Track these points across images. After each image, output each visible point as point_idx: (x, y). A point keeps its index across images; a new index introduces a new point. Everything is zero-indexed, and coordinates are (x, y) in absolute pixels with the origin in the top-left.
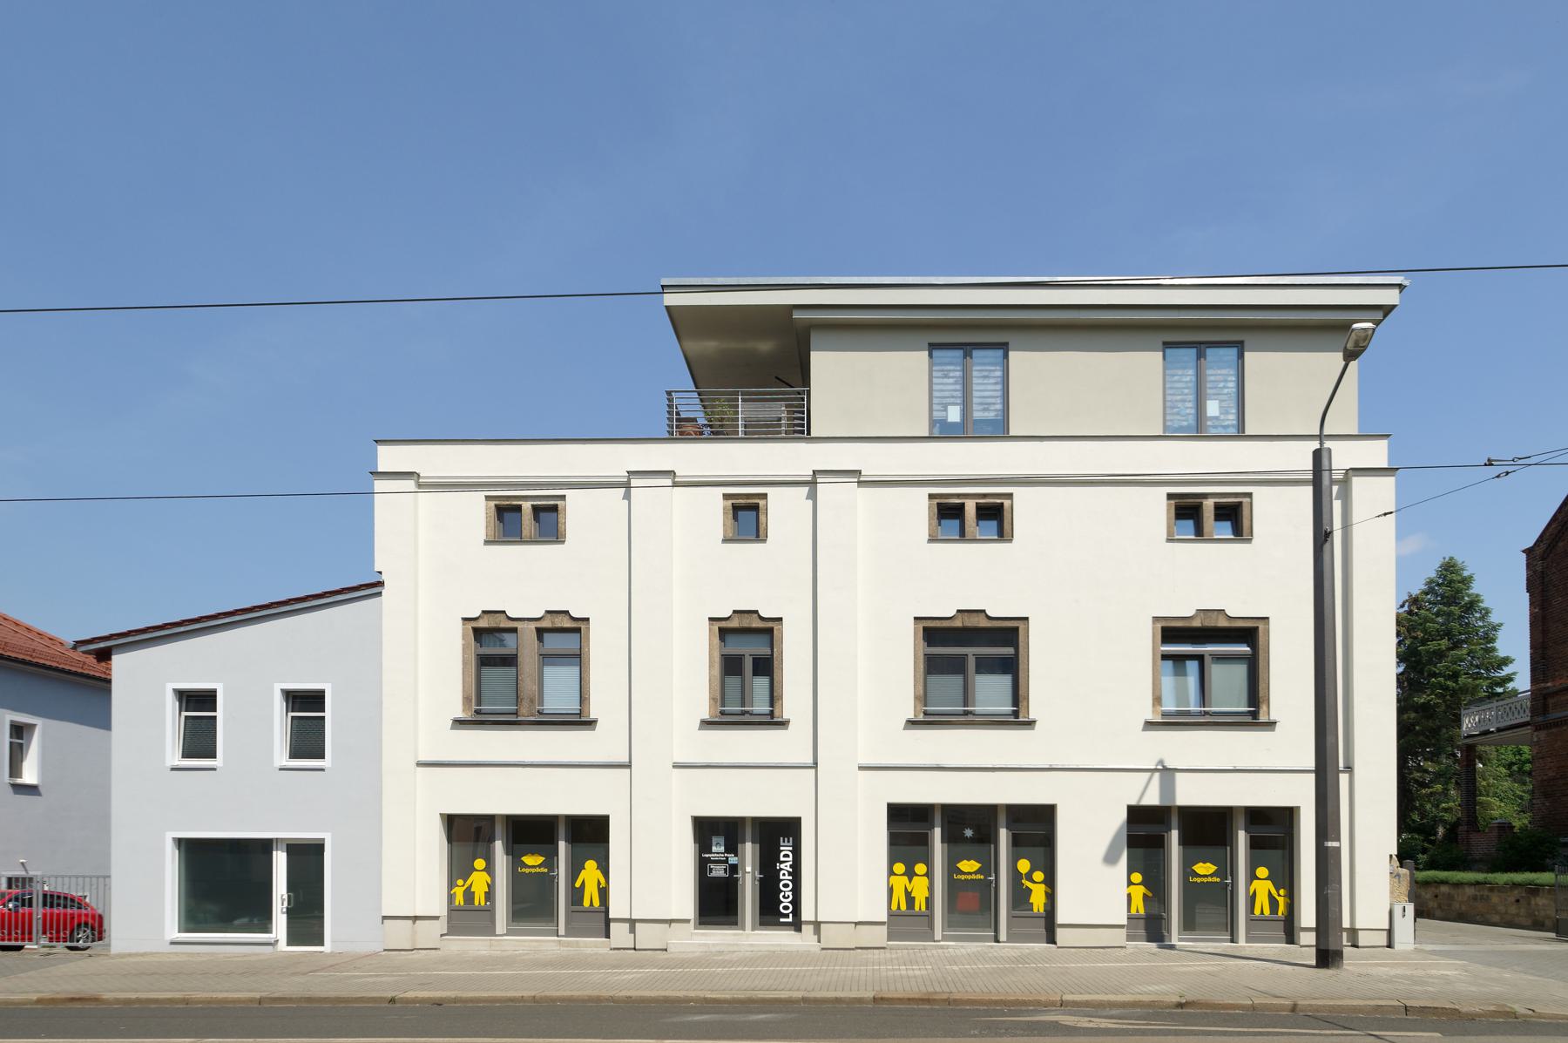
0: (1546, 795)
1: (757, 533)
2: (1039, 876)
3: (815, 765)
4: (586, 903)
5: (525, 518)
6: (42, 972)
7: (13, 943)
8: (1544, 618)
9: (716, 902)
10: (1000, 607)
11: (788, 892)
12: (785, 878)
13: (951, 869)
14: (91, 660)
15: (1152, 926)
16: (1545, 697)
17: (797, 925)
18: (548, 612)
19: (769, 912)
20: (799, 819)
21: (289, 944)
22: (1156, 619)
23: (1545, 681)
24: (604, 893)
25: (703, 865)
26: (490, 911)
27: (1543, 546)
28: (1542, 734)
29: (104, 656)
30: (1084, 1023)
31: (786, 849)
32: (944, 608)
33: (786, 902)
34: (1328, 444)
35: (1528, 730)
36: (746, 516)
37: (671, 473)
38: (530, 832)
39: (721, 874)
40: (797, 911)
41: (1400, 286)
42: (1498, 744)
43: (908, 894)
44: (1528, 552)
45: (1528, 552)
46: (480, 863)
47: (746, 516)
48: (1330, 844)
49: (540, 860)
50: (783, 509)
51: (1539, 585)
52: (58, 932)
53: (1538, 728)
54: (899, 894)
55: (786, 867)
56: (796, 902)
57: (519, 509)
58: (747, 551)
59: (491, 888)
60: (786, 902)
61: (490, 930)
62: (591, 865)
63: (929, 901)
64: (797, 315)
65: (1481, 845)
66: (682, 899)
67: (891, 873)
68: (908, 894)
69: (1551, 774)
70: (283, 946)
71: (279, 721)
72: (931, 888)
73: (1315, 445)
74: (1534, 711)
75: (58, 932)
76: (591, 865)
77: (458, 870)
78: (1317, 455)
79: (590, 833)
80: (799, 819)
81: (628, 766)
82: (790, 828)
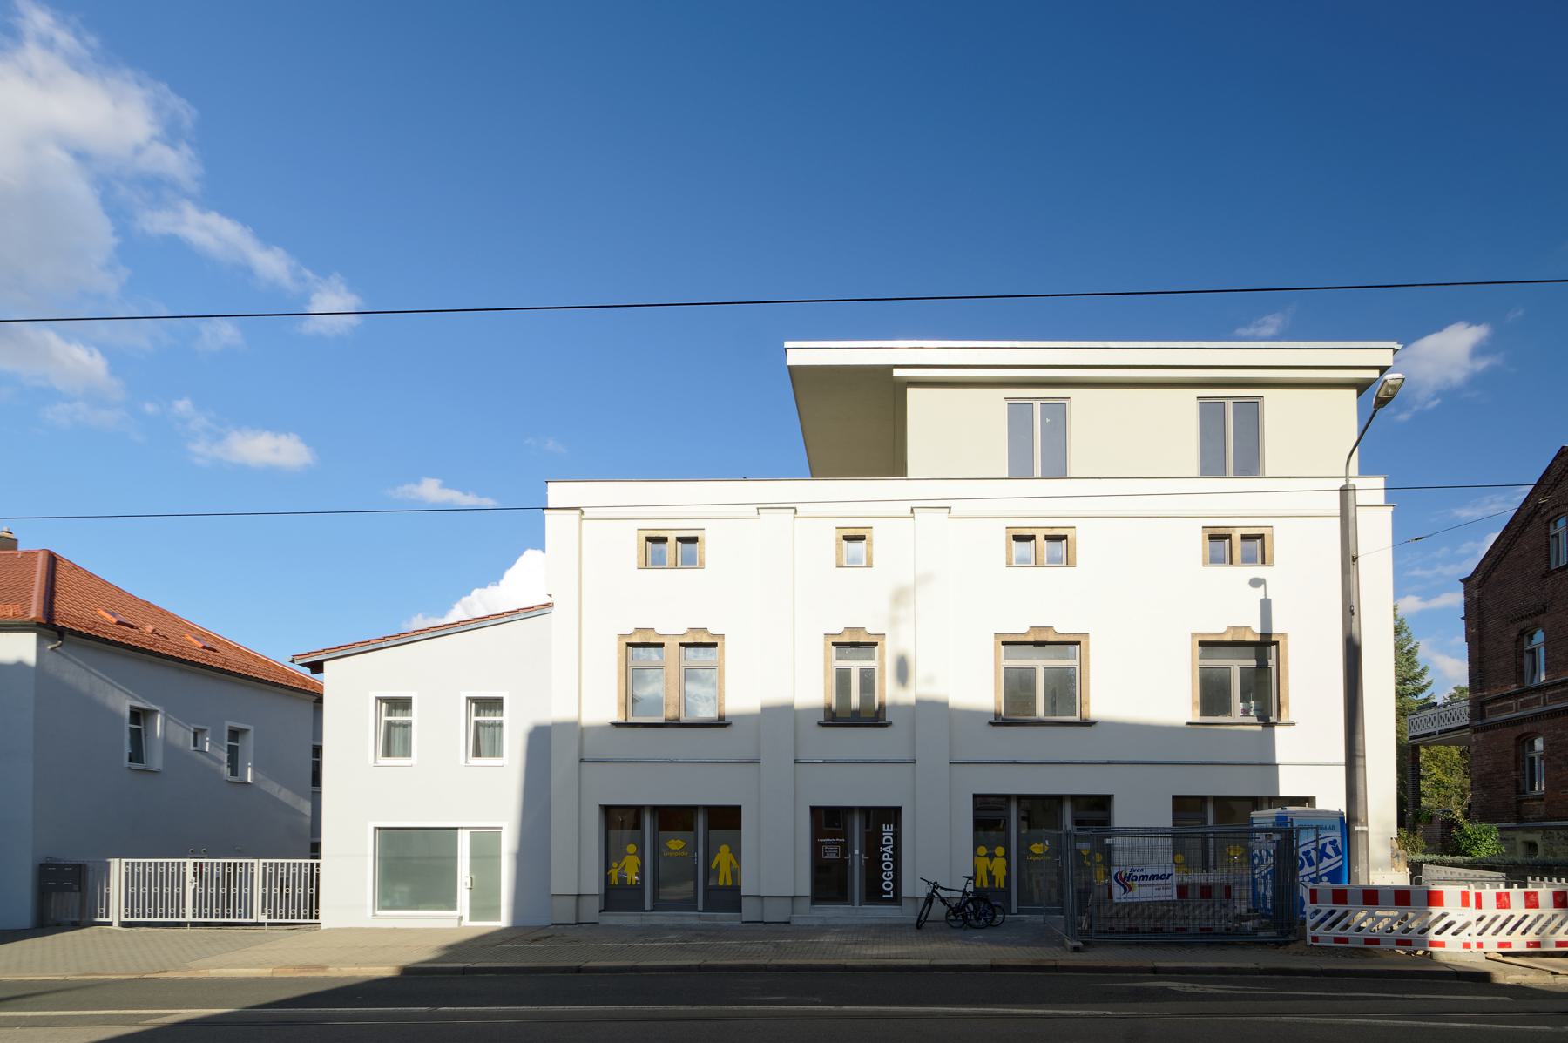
0: (1484, 788)
5: (669, 548)
6: (158, 934)
8: (1481, 638)
9: (829, 882)
10: (1064, 626)
12: (887, 859)
13: (1024, 852)
14: (307, 671)
16: (1483, 704)
17: (897, 900)
19: (874, 893)
22: (1194, 635)
23: (1482, 690)
24: (736, 874)
25: (816, 848)
26: (639, 888)
27: (1479, 577)
28: (1480, 736)
29: (317, 667)
30: (1188, 987)
31: (888, 830)
32: (1019, 626)
33: (888, 881)
34: (1352, 481)
35: (1467, 733)
38: (673, 818)
39: (833, 856)
41: (1395, 351)
42: (1447, 744)
43: (989, 874)
44: (1465, 581)
45: (1465, 581)
46: (632, 848)
48: (1358, 828)
49: (681, 844)
53: (1476, 730)
54: (982, 873)
55: (888, 850)
56: (897, 880)
57: (1228, 537)
60: (888, 881)
62: (724, 849)
63: (1007, 879)
64: (897, 372)
67: (975, 854)
68: (989, 874)
69: (1488, 769)
70: (466, 922)
71: (459, 722)
72: (1008, 868)
73: (1342, 482)
74: (1472, 716)
76: (724, 849)
77: (609, 855)
78: (1344, 491)
79: (726, 818)
82: (892, 815)
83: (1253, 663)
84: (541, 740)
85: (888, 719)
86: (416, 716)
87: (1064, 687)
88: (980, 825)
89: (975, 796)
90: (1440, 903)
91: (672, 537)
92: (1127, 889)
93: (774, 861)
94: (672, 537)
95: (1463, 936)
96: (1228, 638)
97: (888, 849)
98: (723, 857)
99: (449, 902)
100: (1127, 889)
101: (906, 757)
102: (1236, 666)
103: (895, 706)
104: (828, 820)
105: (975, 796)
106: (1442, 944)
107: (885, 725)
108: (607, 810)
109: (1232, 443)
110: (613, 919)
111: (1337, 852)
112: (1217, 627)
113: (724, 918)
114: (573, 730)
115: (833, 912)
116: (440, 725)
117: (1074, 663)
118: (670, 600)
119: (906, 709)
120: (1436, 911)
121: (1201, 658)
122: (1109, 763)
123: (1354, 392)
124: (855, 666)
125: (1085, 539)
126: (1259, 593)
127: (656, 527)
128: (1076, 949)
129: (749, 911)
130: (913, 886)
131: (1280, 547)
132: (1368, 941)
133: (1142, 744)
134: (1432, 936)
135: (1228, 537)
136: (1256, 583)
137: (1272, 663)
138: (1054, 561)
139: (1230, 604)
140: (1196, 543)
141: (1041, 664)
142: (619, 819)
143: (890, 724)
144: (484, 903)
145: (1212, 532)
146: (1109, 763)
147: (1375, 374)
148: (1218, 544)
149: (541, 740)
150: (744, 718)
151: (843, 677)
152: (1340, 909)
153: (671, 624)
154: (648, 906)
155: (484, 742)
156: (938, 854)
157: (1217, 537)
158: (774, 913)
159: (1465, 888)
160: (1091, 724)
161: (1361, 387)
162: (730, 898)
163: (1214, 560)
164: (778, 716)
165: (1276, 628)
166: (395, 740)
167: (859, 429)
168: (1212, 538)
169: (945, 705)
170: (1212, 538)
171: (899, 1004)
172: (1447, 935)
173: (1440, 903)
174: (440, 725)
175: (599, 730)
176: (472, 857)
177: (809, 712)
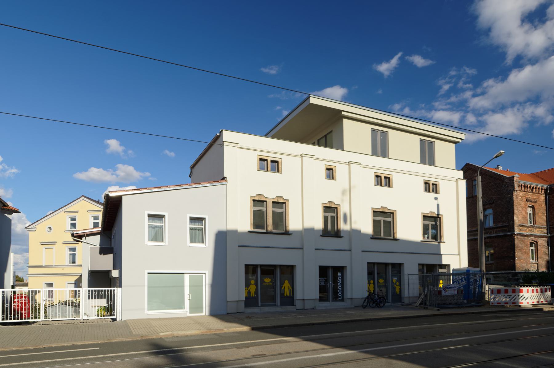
2: (398, 283)
4: (285, 295)
5: (270, 165)
7: (30, 320)
10: (390, 207)
11: (340, 290)
12: (340, 285)
17: (343, 300)
19: (336, 297)
20: (100, 253)
21: (190, 313)
26: (257, 298)
31: (340, 274)
32: (378, 206)
36: (330, 173)
37: (316, 159)
40: (343, 295)
47: (330, 173)
50: (341, 171)
51: (392, 58)
52: (14, 315)
56: (343, 293)
60: (340, 293)
61: (257, 306)
63: (256, 293)
64: (343, 113)
65: (105, 263)
66: (315, 294)
72: (374, 288)
75: (14, 315)
76: (286, 282)
79: (288, 271)
80: (100, 253)
81: (302, 249)
83: (434, 223)
84: (222, 237)
85: (342, 235)
86: (167, 224)
89: (368, 263)
90: (522, 292)
91: (269, 160)
92: (445, 291)
94: (269, 160)
95: (527, 301)
96: (429, 215)
97: (340, 282)
98: (287, 284)
100: (445, 291)
102: (431, 223)
103: (344, 231)
105: (368, 263)
106: (522, 303)
107: (341, 237)
110: (250, 310)
111: (465, 280)
112: (427, 211)
113: (290, 308)
114: (235, 233)
116: (177, 228)
117: (390, 219)
118: (271, 187)
119: (346, 232)
120: (521, 294)
121: (254, 206)
122: (323, 250)
123: (454, 145)
124: (329, 215)
125: (396, 179)
126: (436, 202)
127: (264, 155)
128: (438, 310)
129: (299, 305)
130: (348, 295)
131: (441, 188)
132: (498, 303)
133: (409, 247)
134: (520, 301)
136: (436, 199)
137: (438, 223)
138: (273, 170)
140: (255, 163)
141: (382, 219)
142: (250, 269)
143: (341, 237)
144: (196, 306)
145: (329, 167)
146: (323, 250)
147: (460, 141)
148: (263, 162)
149: (222, 237)
152: (514, 295)
153: (270, 194)
154: (260, 305)
155: (197, 235)
157: (427, 183)
158: (308, 305)
159: (533, 288)
160: (397, 240)
161: (455, 143)
162: (289, 300)
163: (261, 168)
164: (309, 231)
165: (440, 213)
166: (157, 235)
167: (323, 130)
170: (328, 169)
171: (7, 366)
172: (523, 301)
173: (522, 292)
174: (177, 228)
175: (243, 234)
176: (190, 286)
177: (318, 231)
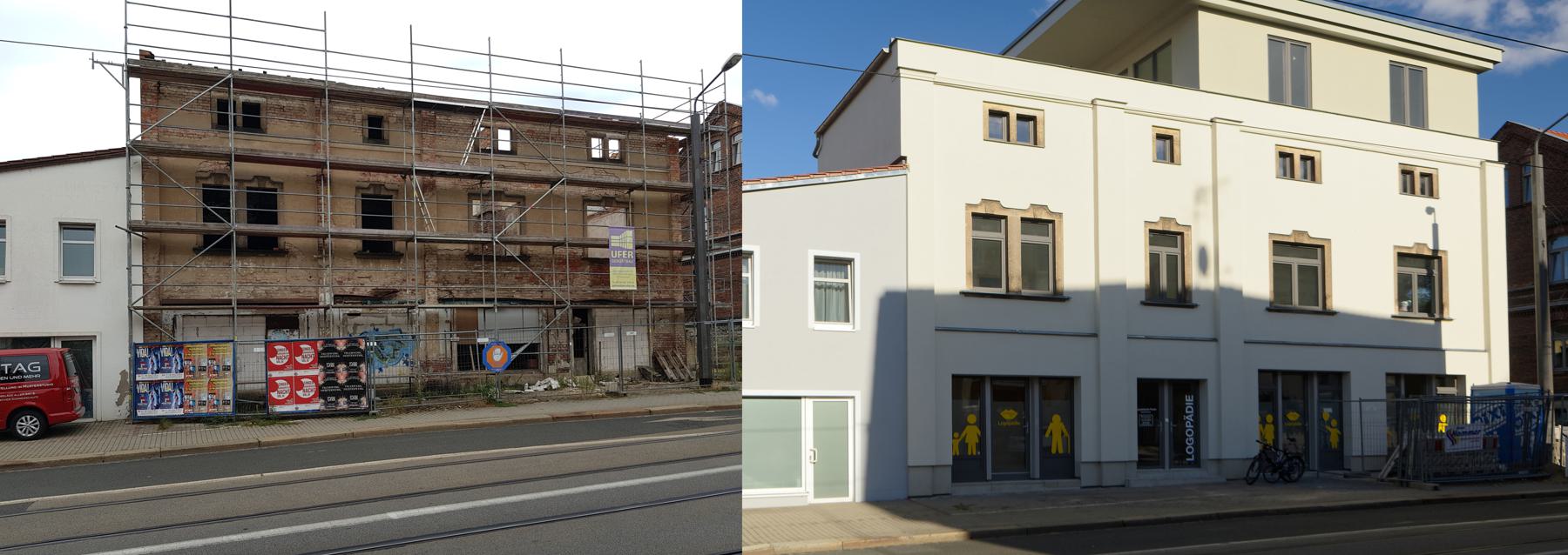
1: (1408, 187)
3: (1487, 350)
5: (1016, 126)
10: (1316, 232)
12: (1189, 426)
15: (1143, 462)
17: (1197, 463)
18: (984, 200)
19: (1180, 458)
21: (816, 496)
31: (1189, 400)
32: (1285, 230)
36: (1166, 146)
40: (1197, 453)
47: (1166, 146)
50: (1191, 142)
55: (1189, 418)
56: (1197, 445)
58: (1167, 167)
59: (982, 438)
60: (1190, 446)
62: (1056, 418)
66: (1128, 448)
71: (51, 244)
76: (1056, 418)
77: (959, 425)
79: (1062, 390)
81: (1095, 335)
82: (1191, 387)
83: (1424, 272)
87: (1041, 260)
88: (1266, 398)
89: (1260, 371)
91: (1013, 113)
92: (1454, 442)
93: (1107, 430)
99: (793, 479)
100: (1454, 442)
101: (1209, 335)
102: (1417, 272)
104: (1148, 391)
105: (1260, 371)
107: (1193, 306)
108: (957, 379)
109: (1409, 104)
110: (965, 489)
112: (1408, 242)
113: (1065, 484)
115: (1152, 476)
117: (1047, 240)
118: (1016, 180)
119: (1206, 293)
121: (975, 228)
123: (1474, 76)
125: (1329, 163)
127: (1290, 144)
128: (1436, 489)
129: (1087, 477)
130: (1210, 451)
131: (1443, 184)
135: (1006, 115)
136: (1430, 211)
137: (1436, 272)
139: (1410, 224)
141: (1295, 262)
142: (966, 387)
144: (830, 481)
147: (1490, 66)
148: (1025, 124)
150: (1082, 295)
151: (1154, 260)
153: (1016, 200)
154: (989, 476)
155: (833, 303)
156: (1233, 425)
157: (1406, 173)
158: (1112, 477)
160: (1333, 313)
162: (1063, 465)
163: (993, 135)
164: (1113, 293)
168: (1159, 137)
169: (1240, 292)
176: (815, 429)
177: (1135, 291)
